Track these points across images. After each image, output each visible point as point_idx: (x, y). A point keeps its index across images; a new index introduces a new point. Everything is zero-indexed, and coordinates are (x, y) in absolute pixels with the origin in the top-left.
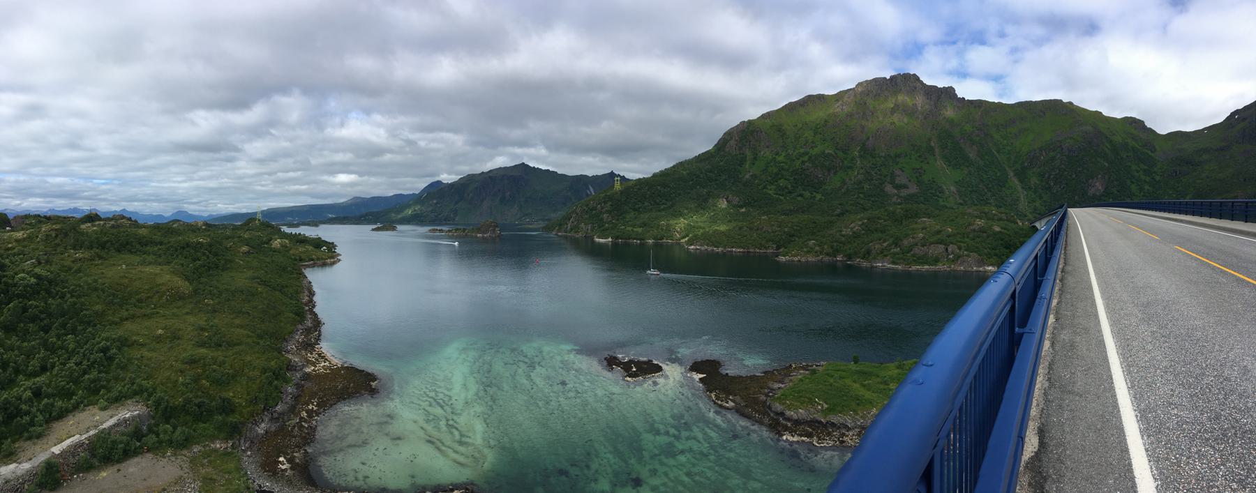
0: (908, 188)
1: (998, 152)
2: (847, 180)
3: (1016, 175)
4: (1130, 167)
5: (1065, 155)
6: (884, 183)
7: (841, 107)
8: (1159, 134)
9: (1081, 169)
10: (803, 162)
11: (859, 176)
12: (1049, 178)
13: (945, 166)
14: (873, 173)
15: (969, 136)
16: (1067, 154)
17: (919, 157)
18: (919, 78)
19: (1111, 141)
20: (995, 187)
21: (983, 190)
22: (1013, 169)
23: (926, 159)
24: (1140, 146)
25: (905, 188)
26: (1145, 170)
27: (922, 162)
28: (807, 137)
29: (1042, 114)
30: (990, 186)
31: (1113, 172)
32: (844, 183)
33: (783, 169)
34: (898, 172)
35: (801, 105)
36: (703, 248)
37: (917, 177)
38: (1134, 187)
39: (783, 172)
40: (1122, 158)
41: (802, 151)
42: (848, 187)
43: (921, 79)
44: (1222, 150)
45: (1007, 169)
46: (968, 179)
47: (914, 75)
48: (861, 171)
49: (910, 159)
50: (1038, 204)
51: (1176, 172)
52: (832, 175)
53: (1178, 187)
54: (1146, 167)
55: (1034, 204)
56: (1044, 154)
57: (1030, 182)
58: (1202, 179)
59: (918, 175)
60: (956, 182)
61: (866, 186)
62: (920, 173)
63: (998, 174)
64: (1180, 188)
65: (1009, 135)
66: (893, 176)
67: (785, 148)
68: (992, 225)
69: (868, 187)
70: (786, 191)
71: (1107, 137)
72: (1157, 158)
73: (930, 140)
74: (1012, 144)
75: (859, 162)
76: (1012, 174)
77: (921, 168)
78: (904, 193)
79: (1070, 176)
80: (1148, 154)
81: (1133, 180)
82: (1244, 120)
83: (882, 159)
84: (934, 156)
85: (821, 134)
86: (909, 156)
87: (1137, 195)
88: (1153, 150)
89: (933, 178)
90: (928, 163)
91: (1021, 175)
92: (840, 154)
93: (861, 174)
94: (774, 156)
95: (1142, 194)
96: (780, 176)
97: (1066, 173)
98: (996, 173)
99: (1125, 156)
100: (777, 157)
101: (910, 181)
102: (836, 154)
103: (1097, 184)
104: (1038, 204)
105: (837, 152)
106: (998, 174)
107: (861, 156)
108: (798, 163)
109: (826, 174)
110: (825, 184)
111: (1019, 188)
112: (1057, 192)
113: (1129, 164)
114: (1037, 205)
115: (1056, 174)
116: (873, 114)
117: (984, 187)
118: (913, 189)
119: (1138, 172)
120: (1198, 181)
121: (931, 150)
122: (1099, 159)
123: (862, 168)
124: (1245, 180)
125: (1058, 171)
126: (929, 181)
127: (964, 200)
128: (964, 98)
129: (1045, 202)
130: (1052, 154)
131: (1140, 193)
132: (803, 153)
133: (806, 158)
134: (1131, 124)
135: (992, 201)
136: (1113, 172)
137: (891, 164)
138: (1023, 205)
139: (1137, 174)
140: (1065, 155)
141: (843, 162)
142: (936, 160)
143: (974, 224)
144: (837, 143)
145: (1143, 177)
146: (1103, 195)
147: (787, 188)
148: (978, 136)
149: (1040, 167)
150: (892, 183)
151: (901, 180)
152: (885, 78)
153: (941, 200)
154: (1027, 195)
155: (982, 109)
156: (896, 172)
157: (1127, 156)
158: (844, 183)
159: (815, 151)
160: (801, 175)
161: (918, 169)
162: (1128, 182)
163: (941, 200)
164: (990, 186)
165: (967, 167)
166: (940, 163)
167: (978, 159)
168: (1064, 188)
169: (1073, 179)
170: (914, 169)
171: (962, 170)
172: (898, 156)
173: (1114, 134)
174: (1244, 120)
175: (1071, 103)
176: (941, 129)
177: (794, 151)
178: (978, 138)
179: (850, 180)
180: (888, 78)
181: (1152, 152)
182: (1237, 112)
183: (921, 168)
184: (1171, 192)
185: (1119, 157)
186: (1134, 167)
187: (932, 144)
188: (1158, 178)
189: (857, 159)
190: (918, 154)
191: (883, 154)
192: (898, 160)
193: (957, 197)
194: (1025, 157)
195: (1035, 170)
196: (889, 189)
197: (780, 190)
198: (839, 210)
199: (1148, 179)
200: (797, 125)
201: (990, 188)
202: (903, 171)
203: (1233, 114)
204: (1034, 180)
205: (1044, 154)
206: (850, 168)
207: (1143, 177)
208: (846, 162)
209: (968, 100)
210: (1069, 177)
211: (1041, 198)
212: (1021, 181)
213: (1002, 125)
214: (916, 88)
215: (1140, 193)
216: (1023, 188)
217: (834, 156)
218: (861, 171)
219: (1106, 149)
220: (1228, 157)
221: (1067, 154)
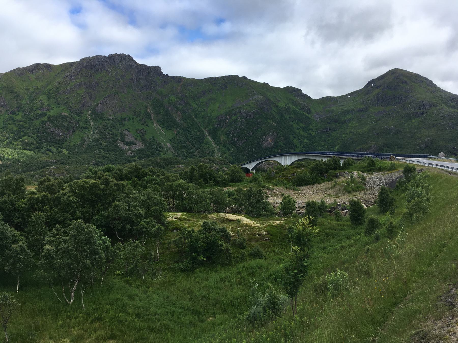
0: (135, 145)
1: (196, 117)
2: (86, 139)
3: (209, 134)
4: (292, 126)
5: (244, 118)
6: (116, 141)
7: (70, 77)
8: (313, 100)
9: (256, 129)
10: (43, 122)
11: (96, 135)
12: (233, 135)
13: (160, 128)
14: (106, 133)
15: (174, 105)
16: (245, 117)
17: (140, 120)
18: (132, 58)
19: (277, 107)
20: (198, 143)
21: (189, 145)
22: (207, 129)
23: (145, 122)
24: (299, 110)
25: (133, 144)
26: (303, 128)
27: (143, 124)
28: (42, 101)
29: (224, 87)
30: (194, 142)
31: (280, 130)
32: (83, 141)
33: (24, 127)
34: (126, 132)
35: (30, 72)
36: (301, 162)
37: (140, 136)
38: (295, 141)
39: (24, 129)
40: (285, 119)
41: (39, 112)
42: (88, 144)
43: (134, 59)
44: (362, 111)
45: (203, 129)
46: (178, 138)
47: (129, 56)
48: (96, 131)
49: (134, 122)
50: (227, 155)
51: (327, 129)
52: (71, 133)
53: (329, 140)
54: (304, 126)
55: (225, 155)
56: (228, 118)
57: (220, 139)
58: (346, 134)
59: (141, 134)
60: (170, 140)
61: (104, 143)
62: (142, 133)
63: (198, 134)
64: (330, 141)
65: (201, 104)
66: (122, 136)
67: (21, 108)
68: (223, 167)
69: (105, 144)
70: (33, 146)
71: (273, 103)
72: (312, 118)
73: (146, 107)
74: (204, 110)
75: (92, 124)
76: (207, 133)
77: (143, 129)
78: (134, 148)
79: (249, 134)
80: (305, 115)
81: (296, 136)
82: (378, 87)
83: (112, 122)
84: (151, 119)
85: (54, 98)
86: (132, 120)
87: (298, 147)
88: (309, 112)
89: (153, 137)
90: (147, 126)
91: (214, 134)
92: (75, 116)
93: (97, 133)
94: (10, 115)
95: (302, 146)
96: (22, 133)
97: (245, 132)
98: (197, 133)
99: (288, 118)
100: (14, 116)
101: (136, 139)
102: (71, 116)
103: (269, 139)
104: (227, 155)
105: (72, 114)
106: (198, 134)
107: (93, 119)
108: (38, 122)
109: (66, 133)
110: (66, 141)
111: (213, 143)
112: (240, 146)
113: (291, 123)
114: (227, 156)
115: (238, 133)
116: (98, 85)
117: (190, 144)
118: (140, 146)
119: (298, 129)
120: (344, 135)
121: (148, 115)
122: (269, 121)
123: (96, 129)
124: (378, 134)
125: (239, 130)
126: (150, 139)
127: (177, 153)
128: (167, 75)
129: (232, 153)
130: (234, 117)
131: (300, 145)
132: (41, 115)
133: (45, 119)
134: (291, 92)
135: (196, 154)
136: (280, 130)
137: (119, 126)
138: (218, 156)
139: (298, 131)
140: (244, 118)
141: (78, 123)
142: (152, 123)
143: (213, 167)
144: (71, 107)
145: (302, 133)
146: (274, 147)
147: (33, 144)
148: (180, 104)
149: (225, 128)
150: (123, 141)
151: (129, 138)
152: (105, 56)
153: (162, 154)
154: (219, 149)
155: (181, 83)
156: (124, 132)
157: (290, 118)
158: (83, 141)
159: (52, 113)
160: (43, 133)
161: (140, 130)
162: (292, 137)
163: (162, 154)
164: (194, 142)
165: (176, 128)
166: (156, 125)
167: (183, 122)
168: (244, 143)
169: (251, 136)
170: (137, 130)
171: (173, 131)
172: (124, 119)
173: (279, 101)
174: (378, 87)
175: (245, 78)
176: (155, 99)
177: (31, 112)
178: (181, 107)
179: (88, 138)
180: (107, 56)
181: (308, 113)
182: (373, 81)
183: (143, 129)
184: (323, 144)
185: (283, 118)
186: (295, 126)
187: (149, 111)
188: (313, 134)
189: (90, 121)
190: (139, 119)
191: (111, 118)
192: (124, 122)
193: (173, 151)
194: (215, 121)
195: (222, 129)
196: (121, 145)
197: (27, 146)
198: (93, 162)
199: (306, 134)
200: (29, 89)
201: (194, 144)
202: (129, 132)
203: (370, 83)
204: (223, 138)
205: (228, 118)
206: (86, 128)
207: (302, 133)
208: (81, 124)
209: (171, 77)
210: (248, 135)
211: (229, 150)
212: (214, 138)
213: (196, 96)
214: (131, 66)
215: (300, 145)
216: (216, 143)
217: (70, 119)
218: (96, 131)
219: (273, 113)
220: (366, 117)
221: (245, 117)
